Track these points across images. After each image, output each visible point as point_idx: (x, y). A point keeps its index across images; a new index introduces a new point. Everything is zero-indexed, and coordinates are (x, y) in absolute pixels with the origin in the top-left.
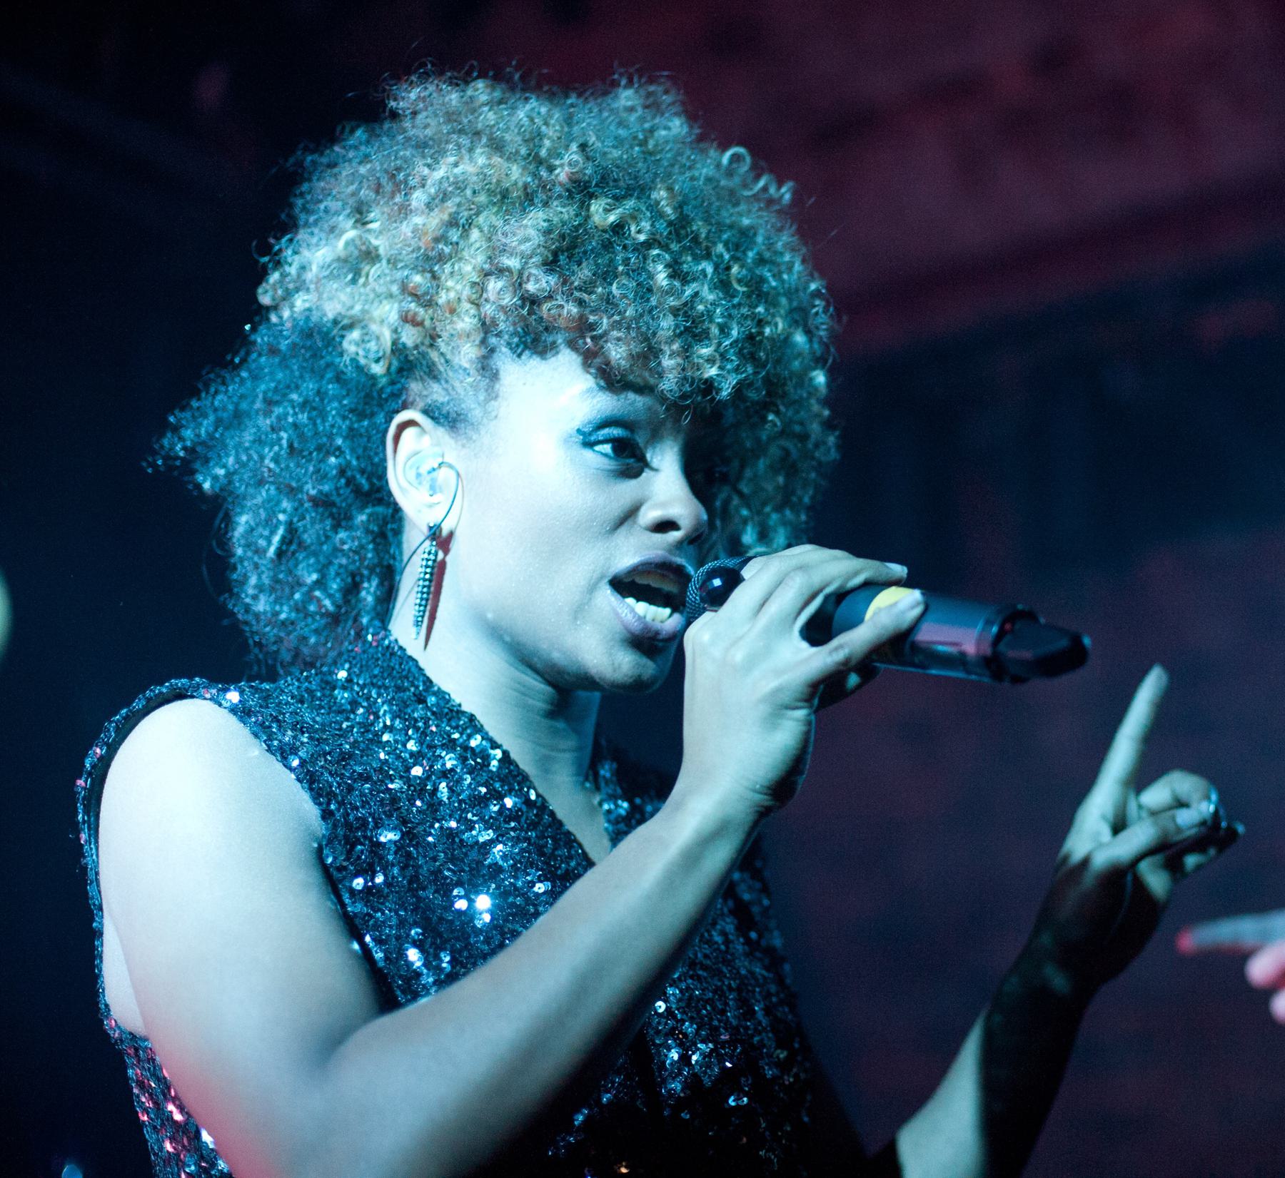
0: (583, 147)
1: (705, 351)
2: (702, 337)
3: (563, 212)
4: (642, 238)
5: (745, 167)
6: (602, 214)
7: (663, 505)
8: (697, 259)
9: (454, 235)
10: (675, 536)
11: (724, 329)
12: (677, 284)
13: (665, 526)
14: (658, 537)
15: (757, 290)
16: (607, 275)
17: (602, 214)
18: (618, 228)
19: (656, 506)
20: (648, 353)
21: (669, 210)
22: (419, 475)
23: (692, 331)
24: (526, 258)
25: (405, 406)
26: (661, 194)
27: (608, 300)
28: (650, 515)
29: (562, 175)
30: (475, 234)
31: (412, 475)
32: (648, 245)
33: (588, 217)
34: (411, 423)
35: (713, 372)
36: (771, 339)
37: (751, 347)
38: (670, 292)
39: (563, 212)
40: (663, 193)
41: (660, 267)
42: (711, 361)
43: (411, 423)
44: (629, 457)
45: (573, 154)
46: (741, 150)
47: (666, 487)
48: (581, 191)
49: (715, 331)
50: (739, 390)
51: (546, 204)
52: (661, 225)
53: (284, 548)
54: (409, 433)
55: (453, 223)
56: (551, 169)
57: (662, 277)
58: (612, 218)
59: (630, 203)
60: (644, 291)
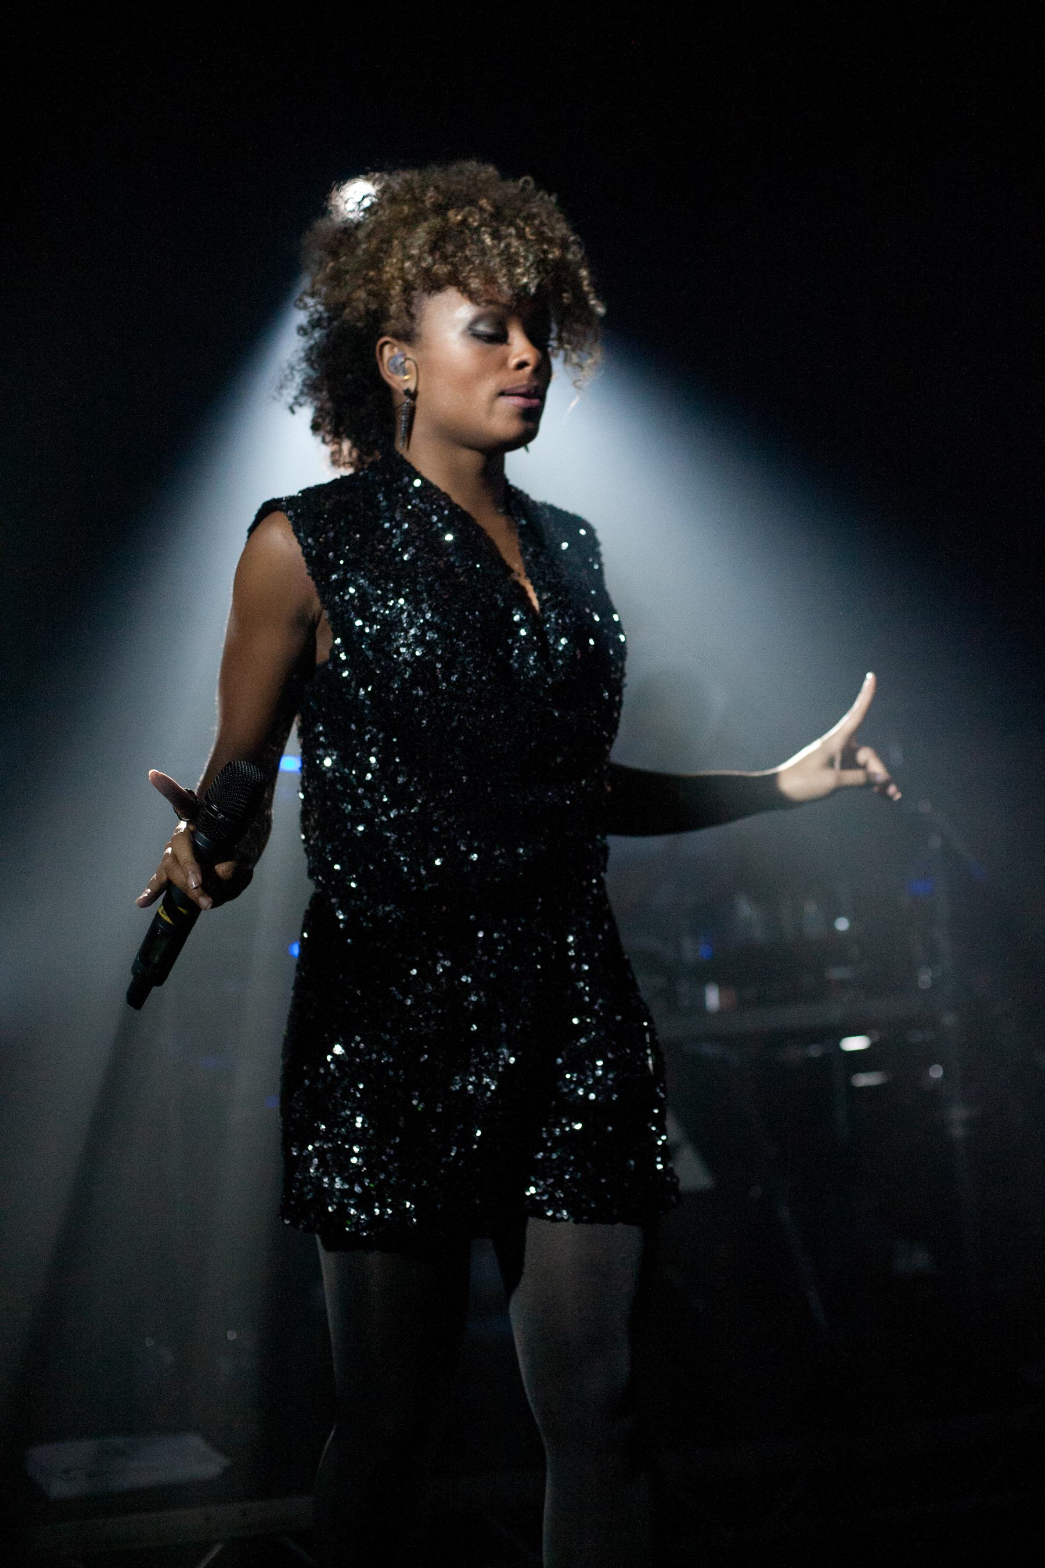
0: (437, 188)
1: (519, 270)
2: (517, 264)
3: (435, 221)
4: (476, 224)
5: (532, 186)
6: (455, 217)
7: (518, 355)
8: (508, 226)
9: (385, 246)
10: (528, 370)
11: (526, 258)
12: (496, 242)
13: (521, 365)
14: (521, 372)
15: (541, 237)
16: (462, 247)
17: (455, 217)
18: (464, 222)
19: (515, 357)
20: (490, 280)
21: (489, 208)
22: (396, 368)
23: (510, 261)
24: (420, 247)
25: (383, 335)
26: (483, 202)
27: (467, 259)
28: (513, 362)
29: (428, 204)
30: (396, 242)
31: (392, 369)
32: (480, 226)
33: (448, 220)
34: (386, 343)
35: (525, 280)
36: (552, 260)
37: (541, 264)
38: (493, 247)
39: (435, 221)
40: (484, 201)
41: (486, 236)
42: (523, 275)
43: (386, 343)
44: (499, 337)
45: (431, 193)
46: (528, 178)
47: (519, 346)
48: (440, 209)
49: (522, 260)
50: (539, 287)
51: (425, 220)
52: (486, 216)
53: (320, 420)
54: (387, 349)
55: (382, 241)
56: (423, 202)
57: (488, 241)
58: (459, 218)
59: (467, 209)
60: (483, 252)
